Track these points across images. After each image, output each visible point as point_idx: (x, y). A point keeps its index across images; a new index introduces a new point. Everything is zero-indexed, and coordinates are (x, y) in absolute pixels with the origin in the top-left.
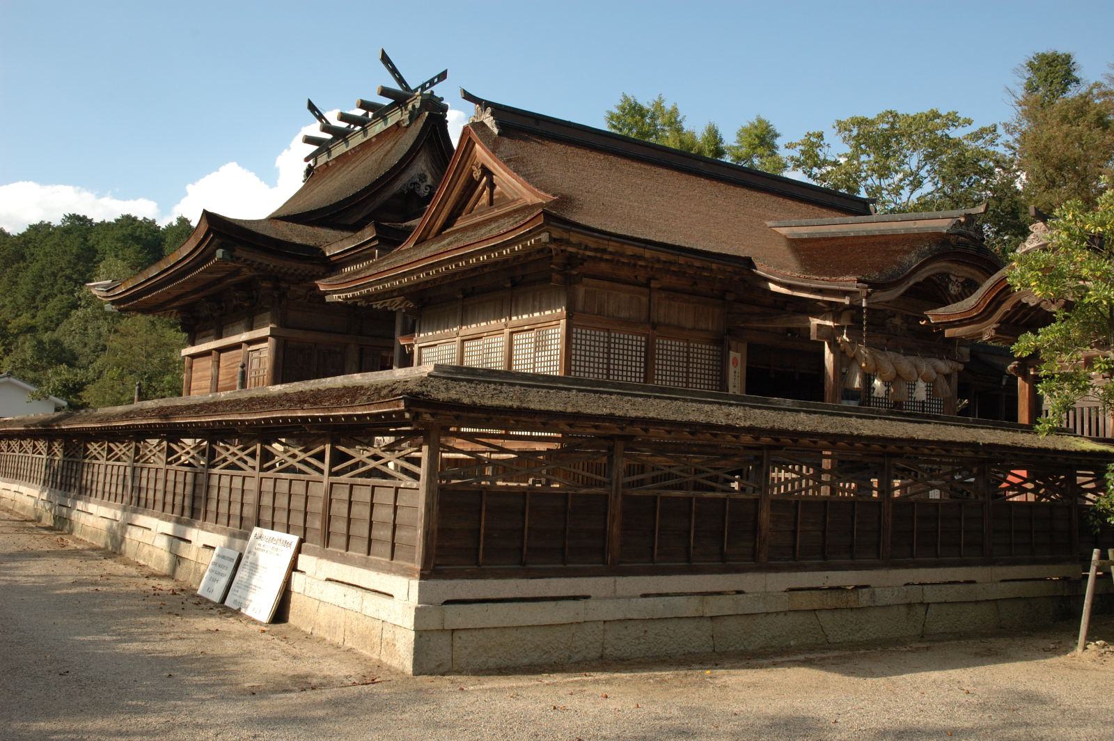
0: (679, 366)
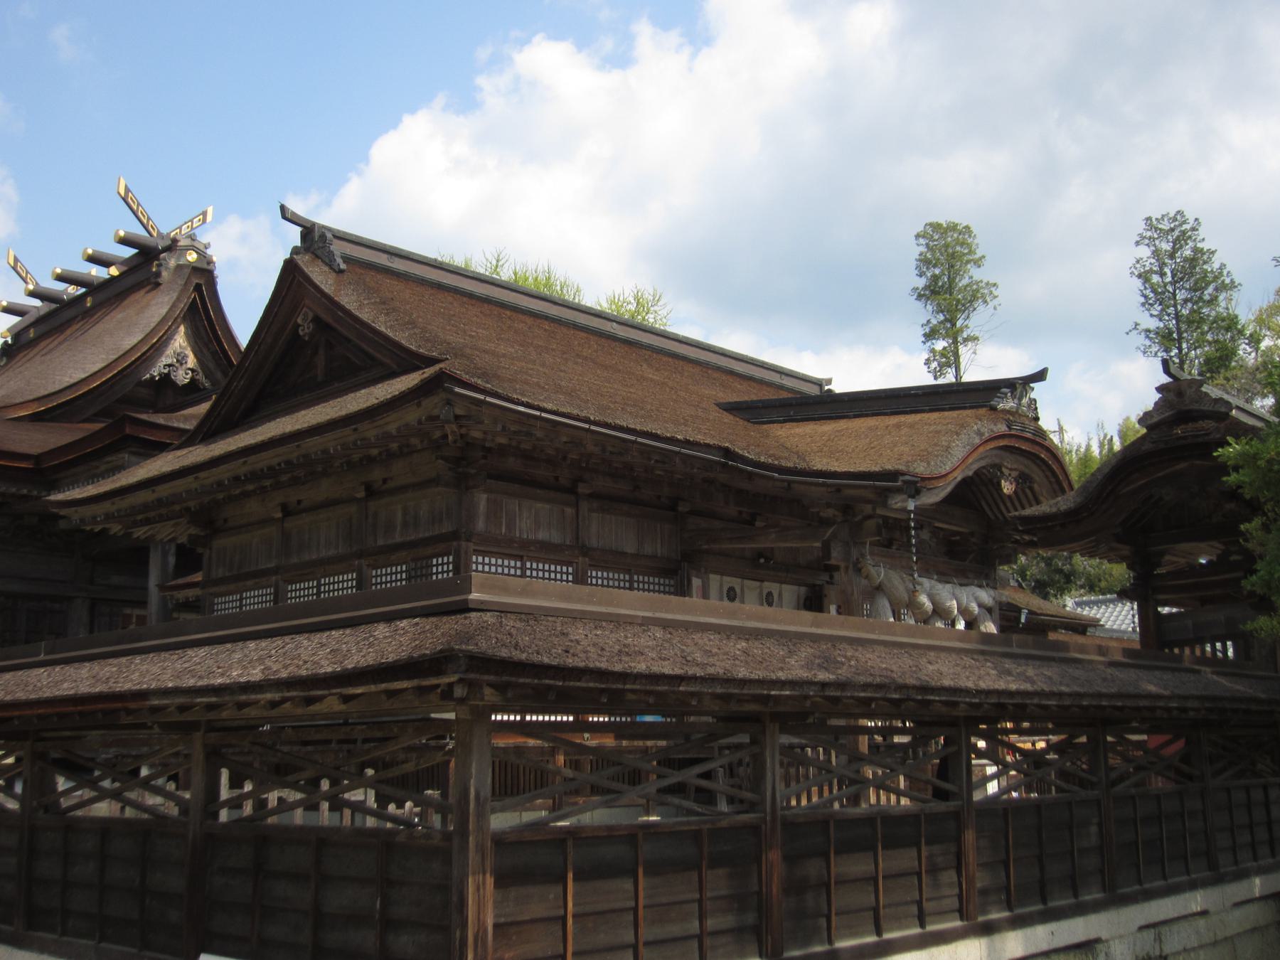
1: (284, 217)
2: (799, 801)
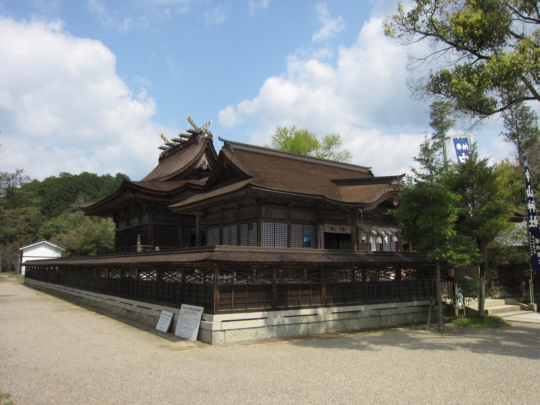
0: (300, 234)
1: (219, 140)
2: (341, 281)
